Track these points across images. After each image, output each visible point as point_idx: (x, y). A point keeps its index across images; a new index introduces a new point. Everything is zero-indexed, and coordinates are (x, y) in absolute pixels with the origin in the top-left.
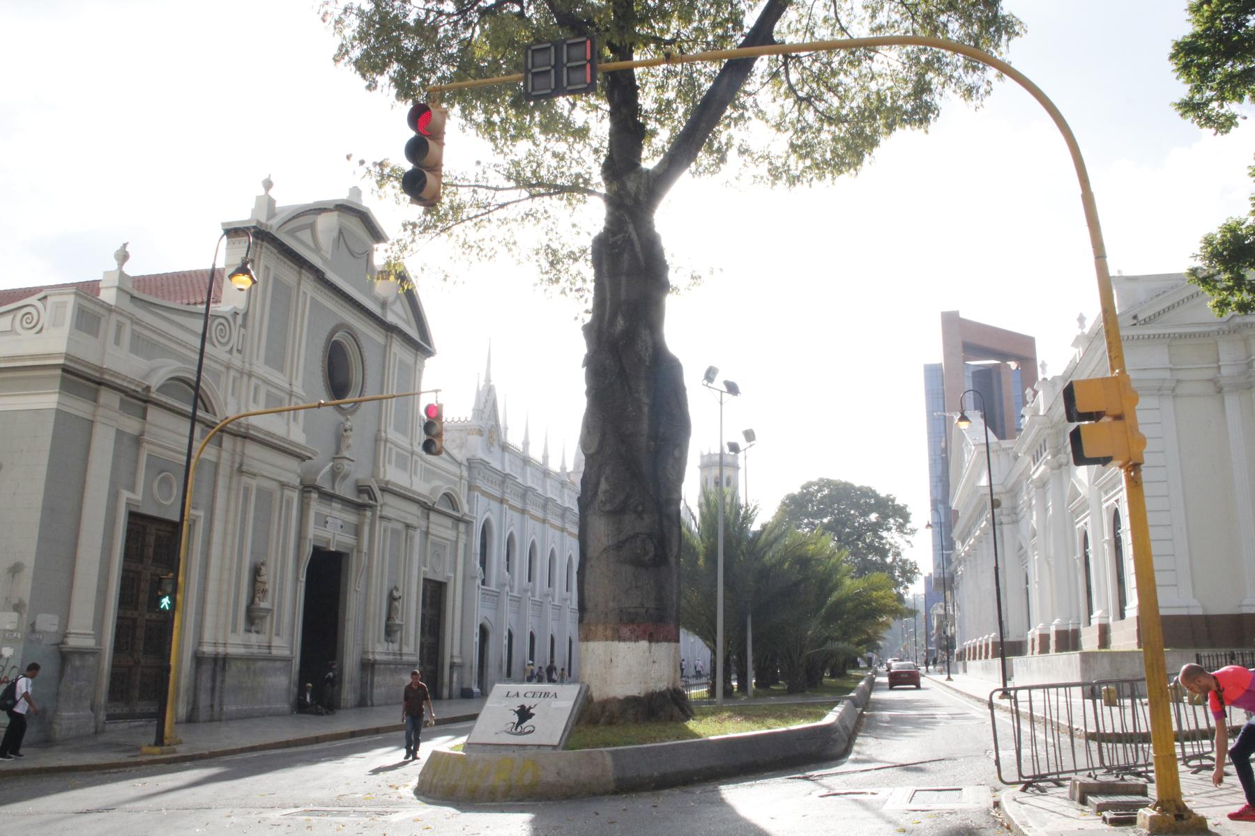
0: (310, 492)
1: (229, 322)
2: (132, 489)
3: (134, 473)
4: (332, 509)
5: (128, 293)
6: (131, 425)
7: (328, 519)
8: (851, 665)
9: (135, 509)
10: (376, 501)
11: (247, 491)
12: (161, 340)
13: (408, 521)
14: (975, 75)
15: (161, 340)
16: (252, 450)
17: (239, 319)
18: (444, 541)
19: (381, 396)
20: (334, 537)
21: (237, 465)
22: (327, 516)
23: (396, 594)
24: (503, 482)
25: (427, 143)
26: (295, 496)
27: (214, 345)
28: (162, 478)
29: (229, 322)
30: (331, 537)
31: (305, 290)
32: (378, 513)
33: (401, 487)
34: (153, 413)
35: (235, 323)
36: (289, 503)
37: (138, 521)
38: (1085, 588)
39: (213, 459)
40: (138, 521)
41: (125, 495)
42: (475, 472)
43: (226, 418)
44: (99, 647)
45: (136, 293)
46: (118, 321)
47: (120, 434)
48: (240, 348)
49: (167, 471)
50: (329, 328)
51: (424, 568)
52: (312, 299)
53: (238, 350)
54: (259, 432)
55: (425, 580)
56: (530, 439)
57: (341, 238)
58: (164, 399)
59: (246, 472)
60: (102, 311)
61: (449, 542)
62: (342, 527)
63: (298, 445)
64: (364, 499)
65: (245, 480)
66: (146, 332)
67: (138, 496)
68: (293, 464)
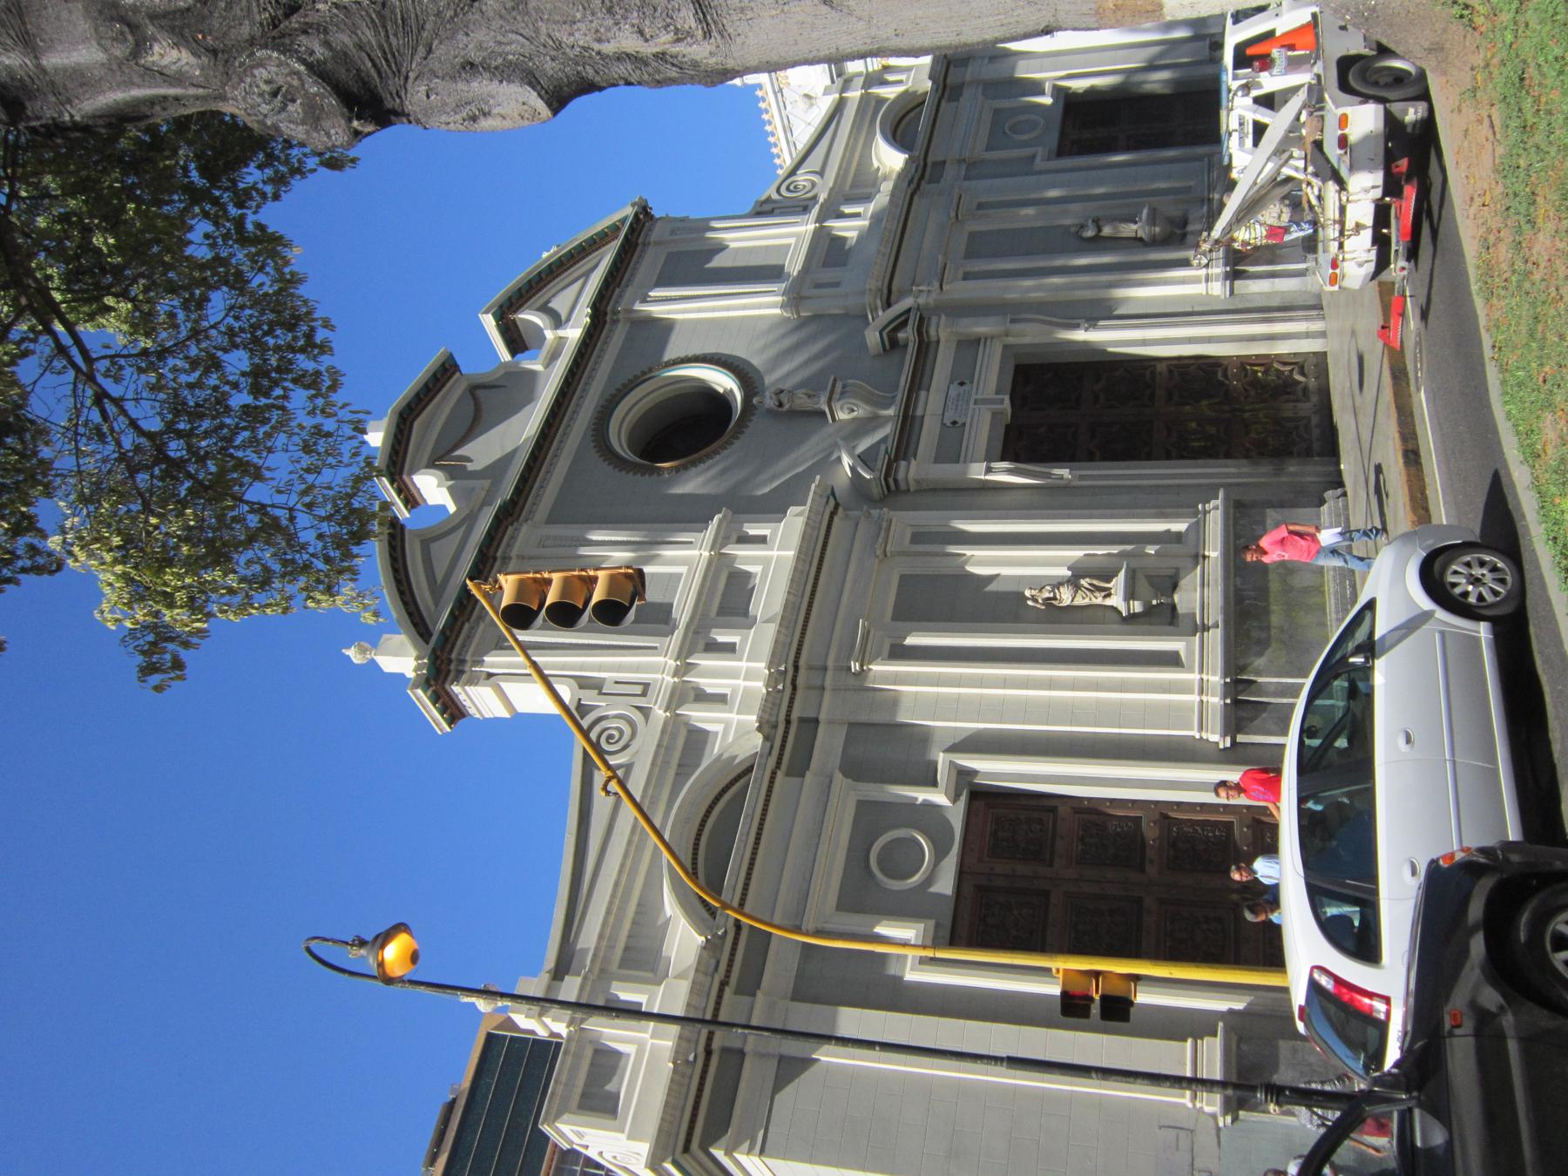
0: (896, 481)
7: (948, 422)
8: (694, 1002)
9: (946, 933)
10: (909, 311)
19: (712, 1028)
20: (985, 401)
22: (943, 424)
25: (381, 419)
28: (882, 870)
38: (837, 140)
43: (842, 393)
44: (1061, 975)
48: (638, 690)
50: (604, 469)
51: (1039, 163)
52: (552, 520)
53: (644, 694)
55: (1061, 152)
58: (921, 140)
62: (962, 384)
64: (908, 334)
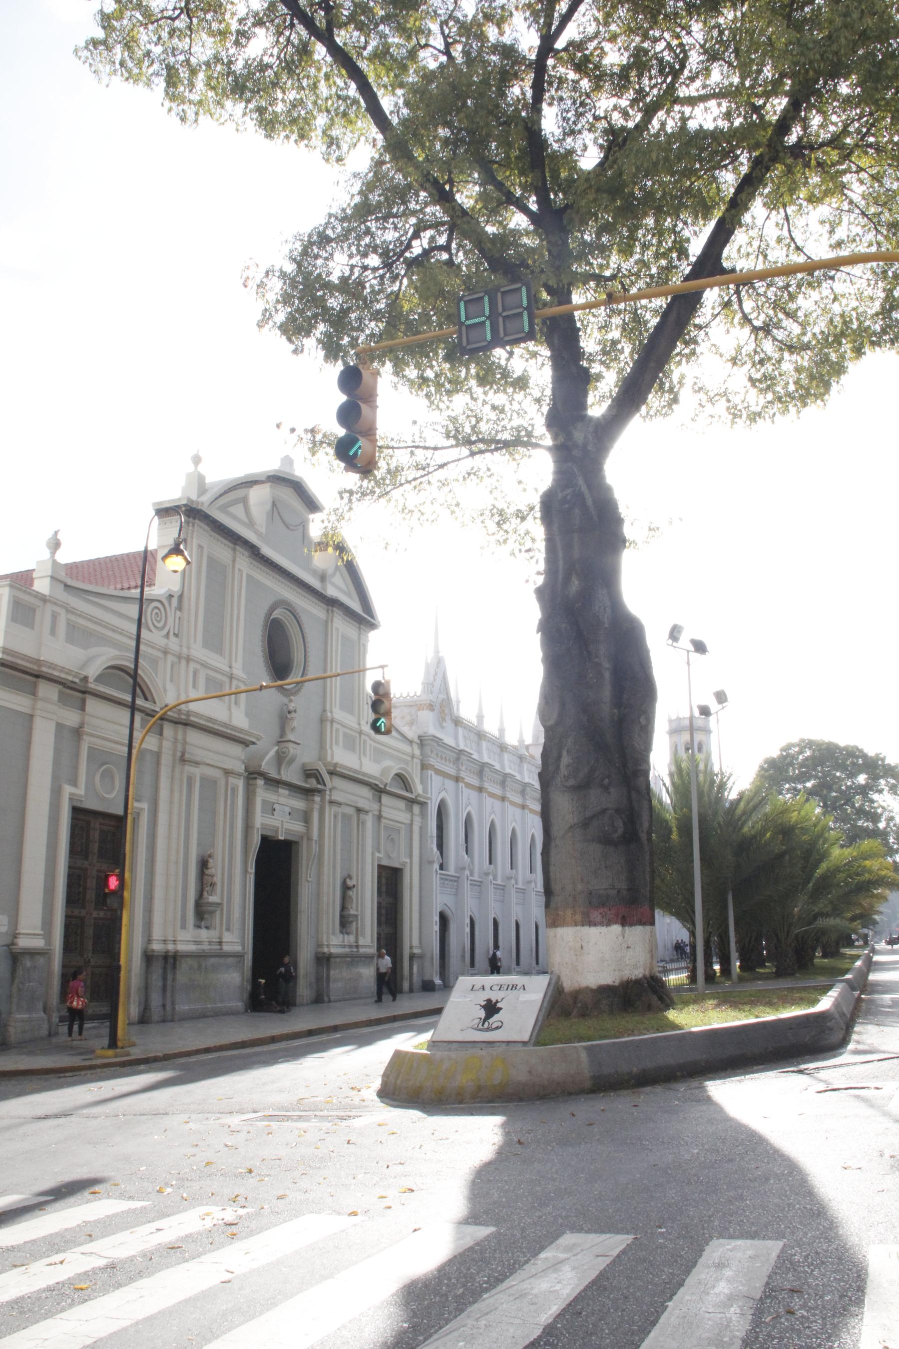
2: (74, 783)
3: (75, 768)
6: (71, 718)
9: (78, 805)
11: (190, 780)
16: (194, 737)
17: (175, 601)
21: (179, 754)
23: (350, 883)
24: (458, 759)
26: (240, 784)
27: (151, 631)
31: (242, 568)
36: (234, 790)
39: (27, 711)
40: (78, 812)
42: (427, 750)
49: (106, 763)
56: (485, 713)
60: (38, 603)
61: (403, 826)
65: (188, 769)
66: (81, 621)
67: (81, 791)
68: (236, 750)
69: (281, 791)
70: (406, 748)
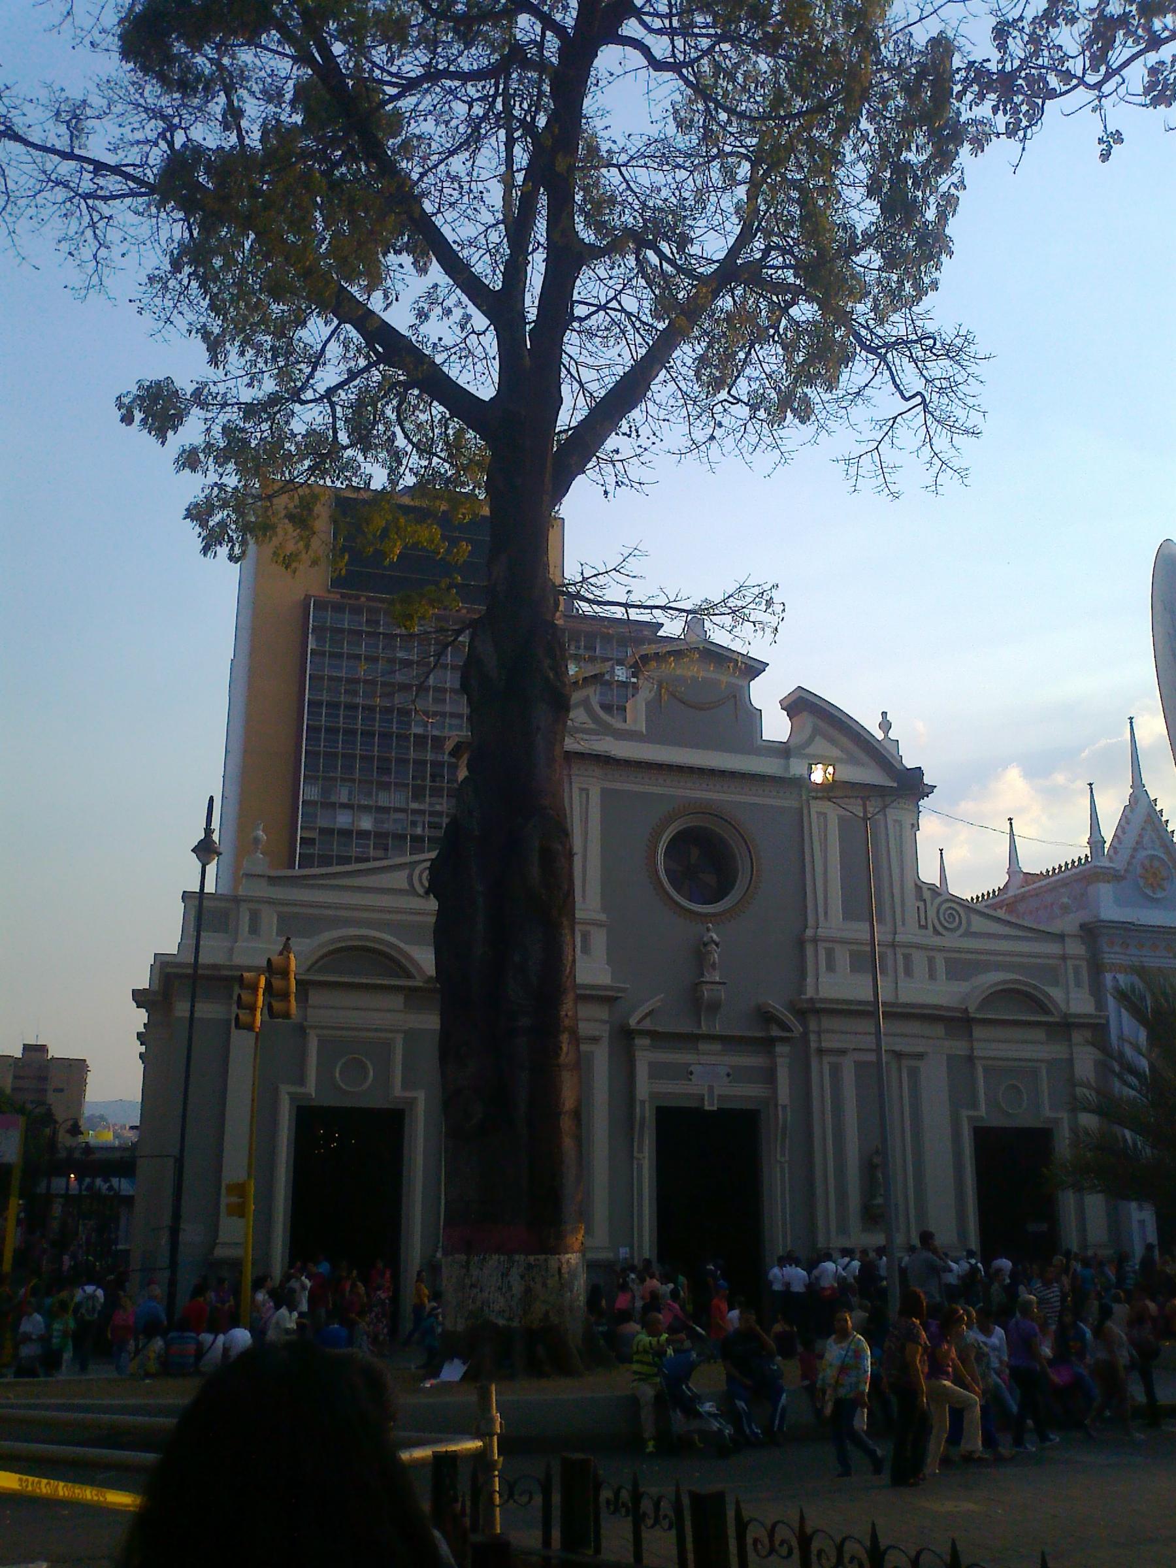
1: (945, 928)
2: (301, 1081)
4: (698, 1054)
5: (262, 876)
6: (959, 1047)
9: (980, 1124)
12: (297, 910)
13: (897, 1048)
14: (865, 175)
15: (297, 910)
18: (383, 1035)
29: (945, 928)
30: (705, 1092)
32: (813, 1045)
33: (935, 1007)
34: (978, 1032)
35: (934, 927)
37: (986, 1138)
40: (986, 1138)
41: (965, 1113)
45: (273, 873)
46: (250, 910)
47: (950, 1058)
51: (965, 1113)
54: (605, 990)
57: (834, 800)
59: (826, 1051)
62: (728, 1075)
63: (605, 988)
69: (702, 1046)
70: (1054, 948)
